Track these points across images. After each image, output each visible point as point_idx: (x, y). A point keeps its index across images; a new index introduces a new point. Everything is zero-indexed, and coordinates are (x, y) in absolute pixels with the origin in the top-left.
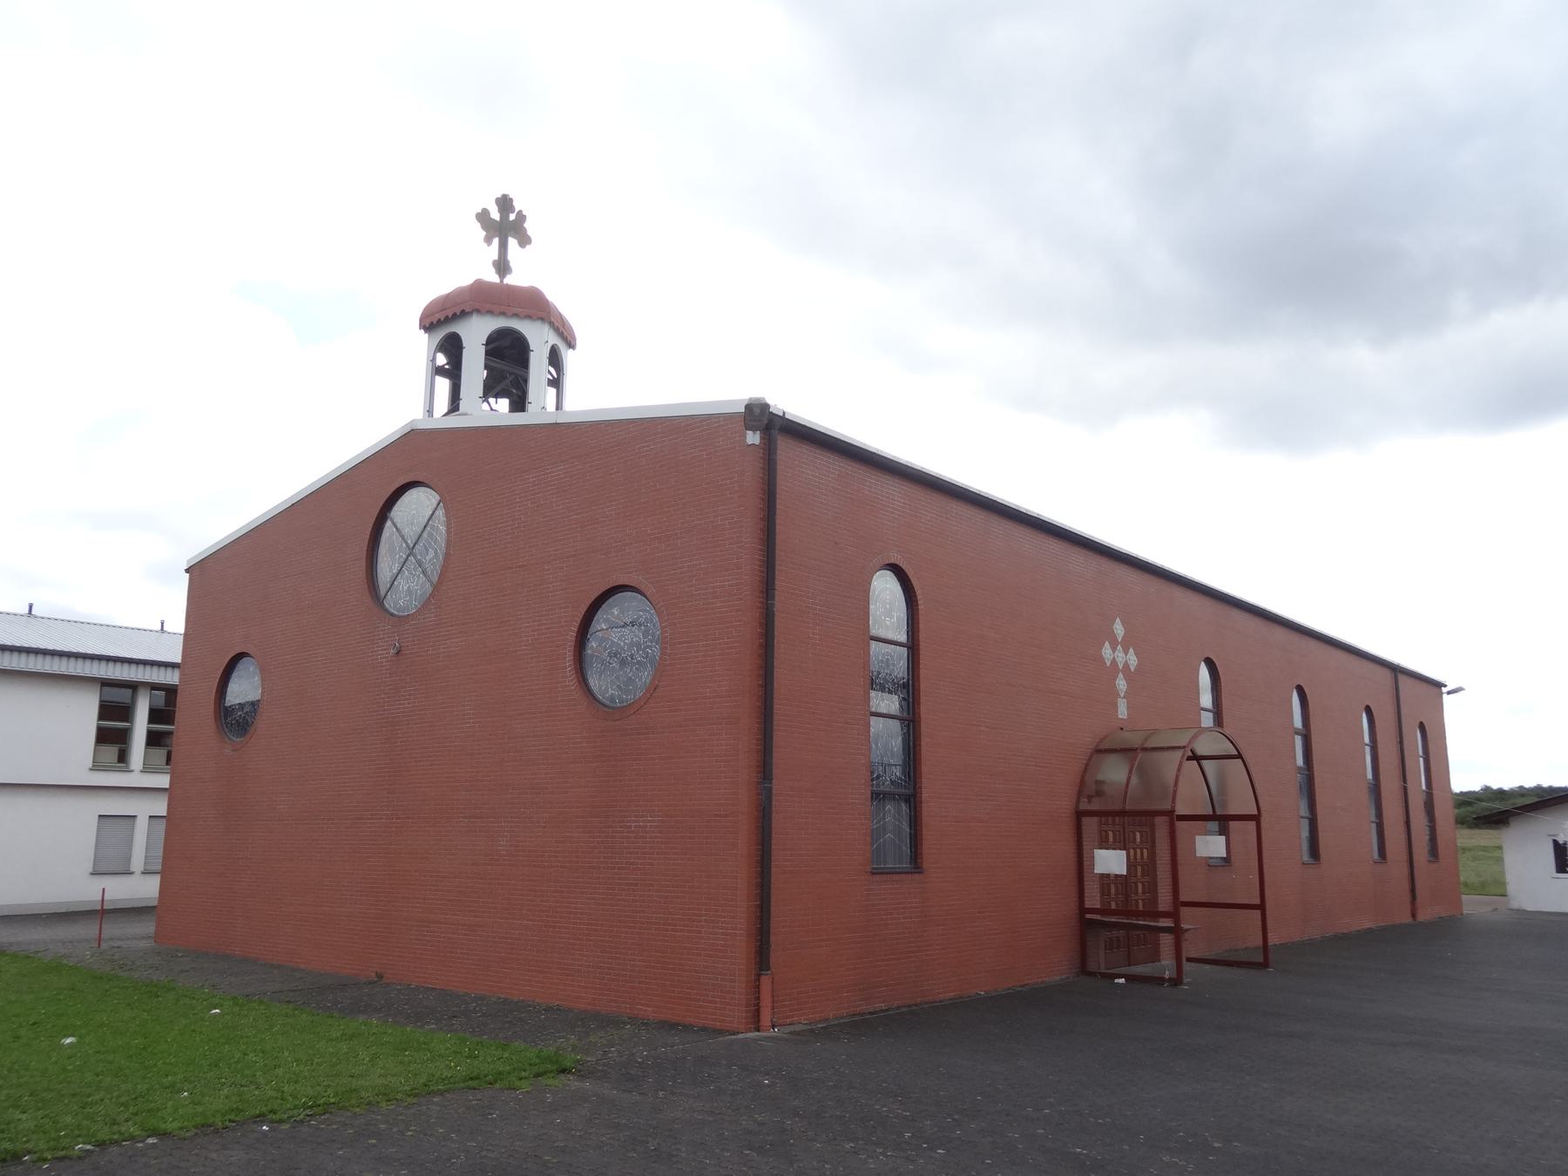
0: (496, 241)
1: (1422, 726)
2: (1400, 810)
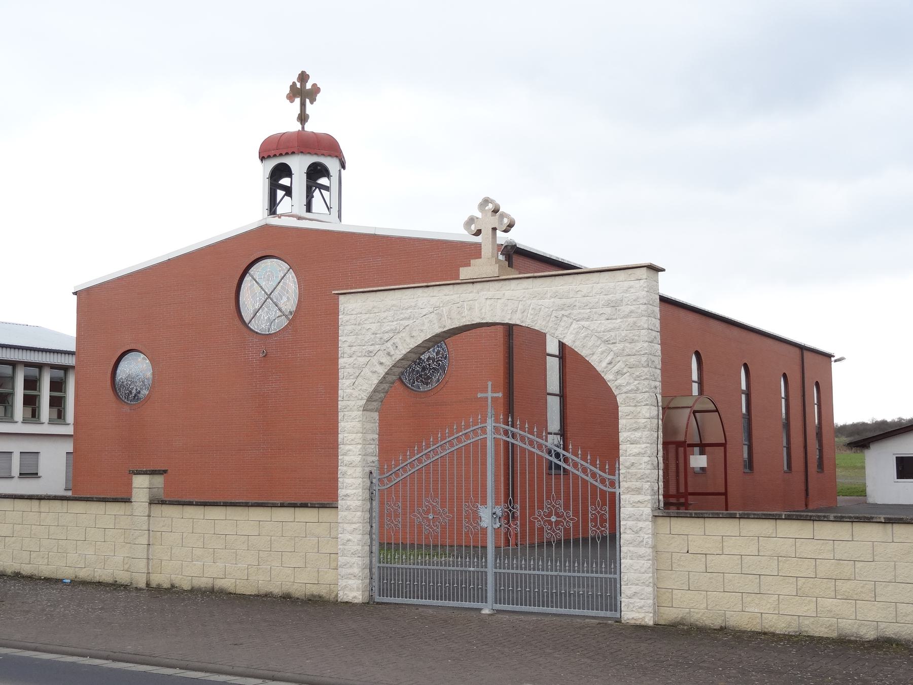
0: (298, 101)
1: (817, 384)
2: (801, 439)
